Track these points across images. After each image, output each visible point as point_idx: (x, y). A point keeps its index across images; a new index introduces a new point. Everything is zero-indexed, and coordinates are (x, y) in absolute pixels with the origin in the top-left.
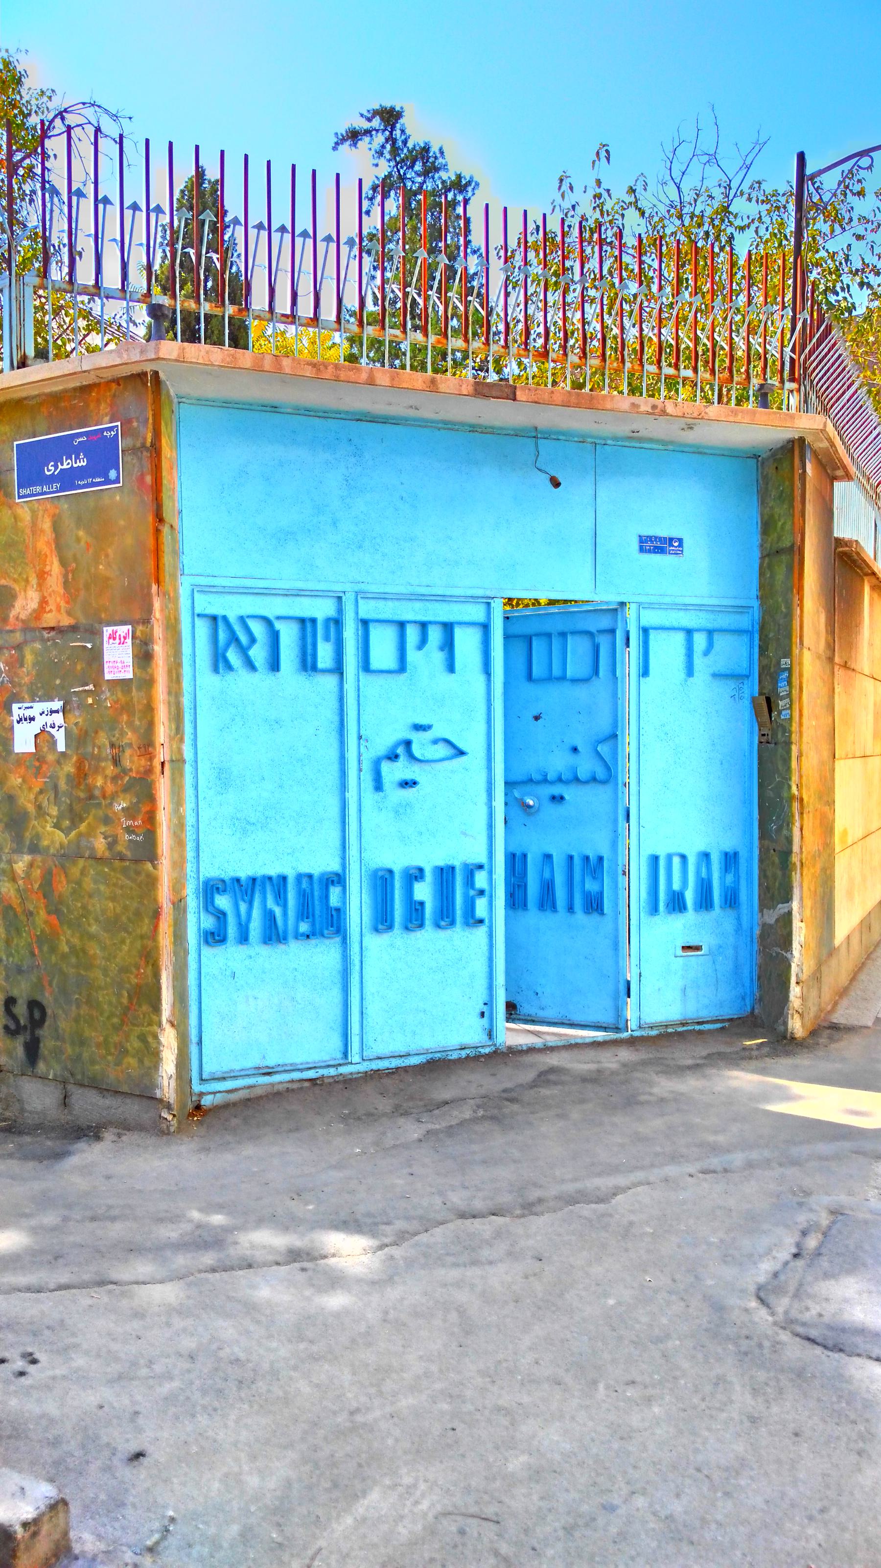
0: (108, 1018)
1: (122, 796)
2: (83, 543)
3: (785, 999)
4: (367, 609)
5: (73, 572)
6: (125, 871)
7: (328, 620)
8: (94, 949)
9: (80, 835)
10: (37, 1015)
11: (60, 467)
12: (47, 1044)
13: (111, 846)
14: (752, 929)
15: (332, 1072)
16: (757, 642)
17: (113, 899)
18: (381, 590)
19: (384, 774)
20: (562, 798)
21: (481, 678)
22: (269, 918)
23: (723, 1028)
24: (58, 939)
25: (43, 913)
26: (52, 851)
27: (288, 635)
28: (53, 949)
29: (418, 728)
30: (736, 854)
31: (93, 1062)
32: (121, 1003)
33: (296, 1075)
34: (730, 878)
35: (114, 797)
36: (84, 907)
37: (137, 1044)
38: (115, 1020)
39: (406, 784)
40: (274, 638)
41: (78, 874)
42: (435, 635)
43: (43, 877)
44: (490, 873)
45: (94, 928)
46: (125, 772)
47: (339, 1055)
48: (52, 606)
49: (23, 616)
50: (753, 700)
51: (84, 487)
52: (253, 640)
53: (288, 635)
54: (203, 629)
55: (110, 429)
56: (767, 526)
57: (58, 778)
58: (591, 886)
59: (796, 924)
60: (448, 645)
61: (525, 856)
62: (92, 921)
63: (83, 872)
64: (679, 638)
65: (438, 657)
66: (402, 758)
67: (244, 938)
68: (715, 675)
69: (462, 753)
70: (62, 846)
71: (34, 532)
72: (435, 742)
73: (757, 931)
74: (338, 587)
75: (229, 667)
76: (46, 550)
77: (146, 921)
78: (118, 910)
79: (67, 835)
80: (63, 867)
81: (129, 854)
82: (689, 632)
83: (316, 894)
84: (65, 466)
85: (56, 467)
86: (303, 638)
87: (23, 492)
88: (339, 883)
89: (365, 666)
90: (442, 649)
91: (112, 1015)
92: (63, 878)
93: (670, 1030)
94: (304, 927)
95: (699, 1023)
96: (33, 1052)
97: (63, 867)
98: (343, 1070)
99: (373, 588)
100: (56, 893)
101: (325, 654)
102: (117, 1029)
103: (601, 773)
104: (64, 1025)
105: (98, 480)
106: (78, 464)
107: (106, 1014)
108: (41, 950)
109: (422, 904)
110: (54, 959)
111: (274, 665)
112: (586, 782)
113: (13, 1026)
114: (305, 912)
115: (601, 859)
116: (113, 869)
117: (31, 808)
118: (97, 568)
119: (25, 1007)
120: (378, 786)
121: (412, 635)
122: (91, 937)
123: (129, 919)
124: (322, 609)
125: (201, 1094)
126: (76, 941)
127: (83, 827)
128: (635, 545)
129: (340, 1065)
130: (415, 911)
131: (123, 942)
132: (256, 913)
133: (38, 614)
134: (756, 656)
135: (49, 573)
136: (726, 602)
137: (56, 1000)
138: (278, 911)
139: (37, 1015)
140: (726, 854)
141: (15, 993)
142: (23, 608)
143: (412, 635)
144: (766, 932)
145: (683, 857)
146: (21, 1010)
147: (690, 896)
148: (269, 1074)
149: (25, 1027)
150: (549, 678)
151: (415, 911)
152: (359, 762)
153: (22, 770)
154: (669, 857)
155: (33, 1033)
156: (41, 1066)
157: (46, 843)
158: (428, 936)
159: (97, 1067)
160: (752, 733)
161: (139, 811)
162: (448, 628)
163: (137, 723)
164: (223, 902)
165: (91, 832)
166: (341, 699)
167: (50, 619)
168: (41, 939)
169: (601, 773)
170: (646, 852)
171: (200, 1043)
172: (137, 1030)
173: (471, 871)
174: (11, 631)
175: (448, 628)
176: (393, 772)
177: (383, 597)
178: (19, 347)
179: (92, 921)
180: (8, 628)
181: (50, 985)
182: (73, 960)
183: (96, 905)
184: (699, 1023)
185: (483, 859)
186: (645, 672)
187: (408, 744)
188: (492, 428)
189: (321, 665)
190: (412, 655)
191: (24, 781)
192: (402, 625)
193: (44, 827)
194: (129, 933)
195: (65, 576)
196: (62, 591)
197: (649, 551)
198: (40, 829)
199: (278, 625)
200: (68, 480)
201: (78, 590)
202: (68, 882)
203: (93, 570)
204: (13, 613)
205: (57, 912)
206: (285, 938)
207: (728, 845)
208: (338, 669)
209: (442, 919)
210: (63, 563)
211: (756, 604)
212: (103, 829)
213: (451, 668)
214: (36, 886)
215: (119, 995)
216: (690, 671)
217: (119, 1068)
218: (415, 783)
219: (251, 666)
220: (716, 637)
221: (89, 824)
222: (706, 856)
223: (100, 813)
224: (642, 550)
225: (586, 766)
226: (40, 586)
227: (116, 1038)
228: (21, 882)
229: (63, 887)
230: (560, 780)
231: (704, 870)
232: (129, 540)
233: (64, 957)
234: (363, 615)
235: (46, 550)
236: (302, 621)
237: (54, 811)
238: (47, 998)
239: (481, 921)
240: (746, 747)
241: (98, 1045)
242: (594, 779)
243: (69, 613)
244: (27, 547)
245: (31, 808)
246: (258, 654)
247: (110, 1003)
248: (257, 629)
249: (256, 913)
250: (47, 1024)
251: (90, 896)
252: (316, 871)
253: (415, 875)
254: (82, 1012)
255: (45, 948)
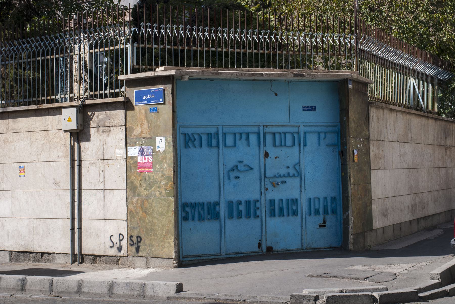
0: (160, 239)
1: (163, 181)
2: (153, 117)
3: (348, 240)
4: (225, 130)
5: (150, 124)
6: (164, 200)
7: (215, 133)
8: (155, 221)
9: (152, 191)
10: (139, 240)
11: (147, 97)
12: (142, 247)
13: (160, 194)
14: (341, 220)
15: (217, 257)
16: (340, 135)
17: (161, 207)
18: (229, 125)
19: (230, 175)
20: (286, 182)
21: (258, 148)
22: (200, 214)
23: (331, 250)
24: (146, 219)
25: (141, 212)
26: (144, 196)
27: (204, 138)
28: (144, 222)
29: (240, 162)
30: (335, 198)
31: (156, 251)
32: (163, 234)
33: (207, 258)
34: (334, 205)
35: (161, 181)
36: (153, 210)
37: (167, 245)
38: (161, 239)
39: (237, 177)
40: (201, 138)
41: (151, 202)
42: (244, 136)
43: (141, 203)
44: (261, 203)
45: (156, 215)
46: (164, 174)
47: (219, 253)
48: (144, 132)
49: (136, 135)
50: (339, 152)
51: (154, 102)
52: (195, 140)
53: (204, 138)
54: (182, 137)
55: (161, 89)
56: (341, 102)
57: (146, 177)
58: (294, 208)
59: (350, 217)
60: (248, 139)
61: (274, 200)
62: (155, 213)
63: (153, 201)
64: (316, 135)
65: (245, 142)
66: (235, 170)
67: (193, 219)
68: (327, 145)
69: (252, 169)
70: (147, 194)
71: (139, 113)
72: (245, 166)
73: (342, 221)
74: (218, 124)
75: (189, 147)
76: (143, 118)
77: (170, 212)
78: (162, 210)
79: (148, 191)
80: (147, 200)
81: (165, 195)
82: (319, 133)
83: (212, 208)
84: (149, 97)
85: (146, 97)
86: (208, 138)
87: (136, 103)
88: (218, 205)
89: (225, 145)
90: (246, 140)
91: (161, 238)
92: (147, 202)
93: (316, 250)
94: (209, 217)
95: (325, 248)
96: (138, 250)
97: (147, 200)
98: (220, 257)
99: (226, 124)
100: (145, 207)
101: (214, 142)
102: (162, 241)
103: (296, 175)
104: (147, 242)
105: (157, 101)
106: (152, 97)
107: (159, 238)
108: (140, 222)
109: (241, 211)
110: (144, 224)
111: (201, 146)
112: (283, 177)
113: (132, 243)
114: (209, 213)
115: (297, 200)
116: (161, 200)
117: (138, 185)
118: (157, 123)
119: (136, 238)
120: (229, 178)
121: (238, 136)
122: (155, 218)
123: (165, 213)
124: (213, 130)
125: (183, 261)
126: (151, 219)
127: (153, 189)
128: (302, 109)
129: (219, 255)
130: (239, 213)
131: (164, 218)
132: (197, 213)
133: (140, 134)
134: (340, 139)
135: (144, 124)
136: (329, 124)
137: (145, 235)
138: (202, 213)
139: (139, 240)
140: (332, 198)
141: (133, 234)
142: (136, 133)
143: (238, 136)
144: (344, 219)
145: (319, 199)
146: (134, 239)
147: (321, 211)
148: (200, 257)
149: (136, 243)
150: (281, 145)
151: (239, 213)
152: (224, 172)
153: (135, 175)
154: (315, 198)
155: (138, 244)
156: (140, 253)
157: (142, 194)
158: (244, 220)
159: (156, 252)
160: (339, 162)
161: (168, 184)
162: (248, 134)
163: (168, 162)
164: (188, 209)
165: (155, 190)
166: (218, 155)
167: (143, 136)
168: (140, 219)
169: (296, 175)
170: (308, 197)
171: (182, 247)
172: (168, 241)
173: (256, 201)
174: (133, 138)
175: (248, 134)
176: (232, 175)
177: (230, 126)
178: (132, 63)
179: (155, 213)
180: (132, 138)
181: (143, 231)
182: (150, 224)
183: (156, 209)
184: (325, 248)
185: (259, 198)
186: (305, 145)
187: (237, 166)
188: (204, 255)
189: (213, 145)
190: (238, 142)
191: (136, 177)
192: (235, 134)
193: (142, 190)
194: (165, 216)
195: (148, 125)
196: (147, 129)
197: (306, 110)
198: (140, 190)
199: (201, 135)
200: (149, 100)
201: (152, 128)
202: (148, 203)
203: (156, 123)
204: (133, 134)
205: (145, 212)
206: (204, 220)
207: (333, 194)
208: (217, 146)
209: (247, 216)
210: (148, 121)
211: (339, 124)
212: (158, 189)
213: (249, 145)
214: (139, 205)
215: (163, 232)
216: (319, 145)
217: (162, 252)
218: (239, 177)
219: (195, 146)
220: (327, 134)
221: (154, 188)
222: (326, 198)
223: (158, 185)
224: (303, 110)
225: (292, 171)
226: (141, 127)
227: (162, 244)
228: (135, 204)
229: (147, 205)
230: (284, 176)
231: (325, 203)
232: (166, 116)
233: (147, 223)
234: (224, 131)
235: (143, 118)
236: (208, 134)
237: (145, 185)
238: (142, 235)
239: (258, 216)
240: (338, 166)
241: (157, 246)
242: (294, 175)
243: (149, 134)
244: (137, 117)
245: (138, 185)
246: (197, 143)
247: (160, 235)
248: (196, 137)
249: (197, 213)
250: (142, 241)
251: (155, 207)
252: (212, 202)
253: (239, 203)
254: (152, 238)
255: (142, 222)
